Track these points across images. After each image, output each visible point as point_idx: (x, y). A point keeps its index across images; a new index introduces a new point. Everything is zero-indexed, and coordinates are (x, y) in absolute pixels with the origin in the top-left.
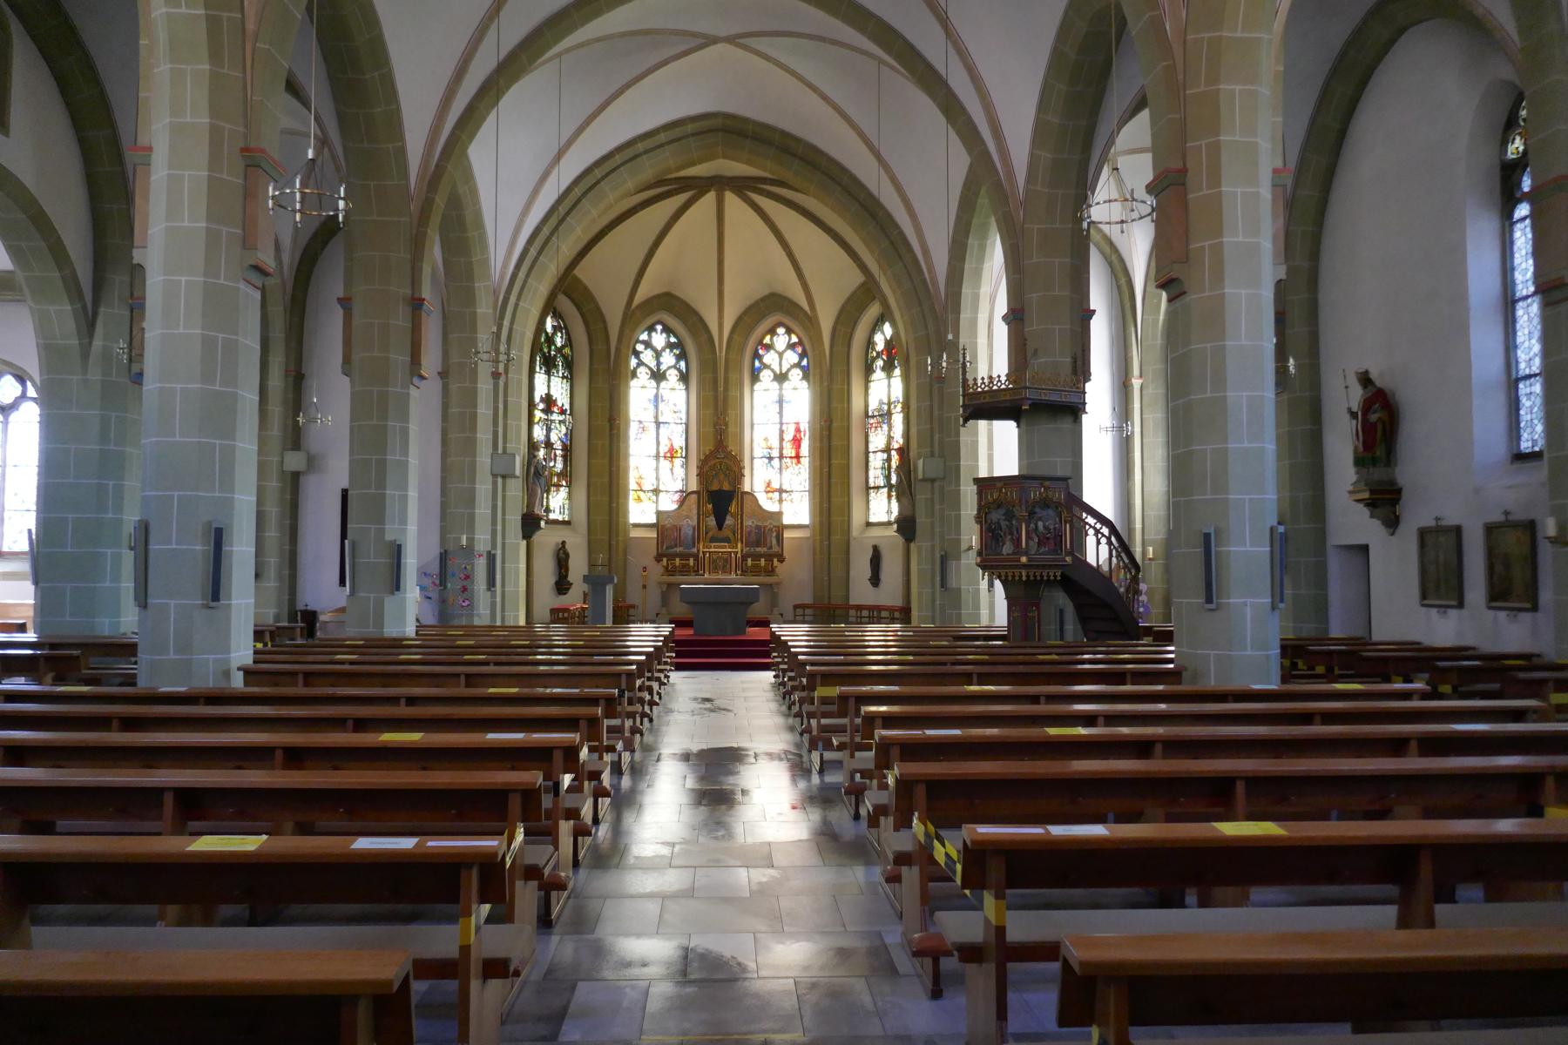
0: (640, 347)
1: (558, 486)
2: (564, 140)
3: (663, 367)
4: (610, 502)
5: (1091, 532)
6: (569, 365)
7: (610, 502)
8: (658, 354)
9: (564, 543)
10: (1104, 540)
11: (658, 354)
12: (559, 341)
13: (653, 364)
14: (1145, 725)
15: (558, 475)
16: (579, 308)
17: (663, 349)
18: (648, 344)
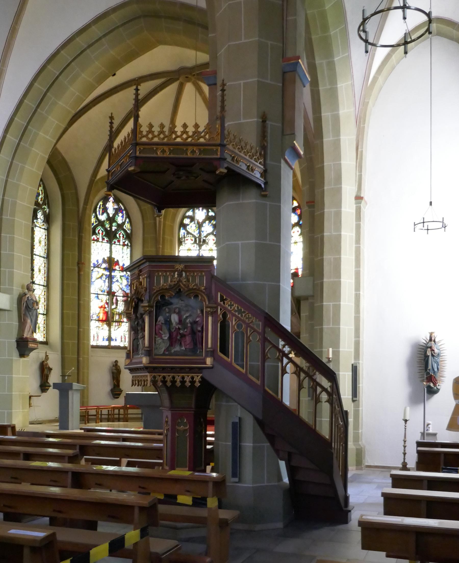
0: (186, 221)
1: (119, 322)
2: (379, 9)
3: (204, 234)
4: (79, 300)
5: (290, 368)
6: (129, 237)
7: (79, 300)
8: (200, 226)
9: (116, 362)
10: (324, 396)
11: (200, 226)
12: (120, 219)
13: (196, 233)
14: (67, 439)
15: (120, 314)
16: (61, 189)
17: (204, 221)
18: (192, 219)
